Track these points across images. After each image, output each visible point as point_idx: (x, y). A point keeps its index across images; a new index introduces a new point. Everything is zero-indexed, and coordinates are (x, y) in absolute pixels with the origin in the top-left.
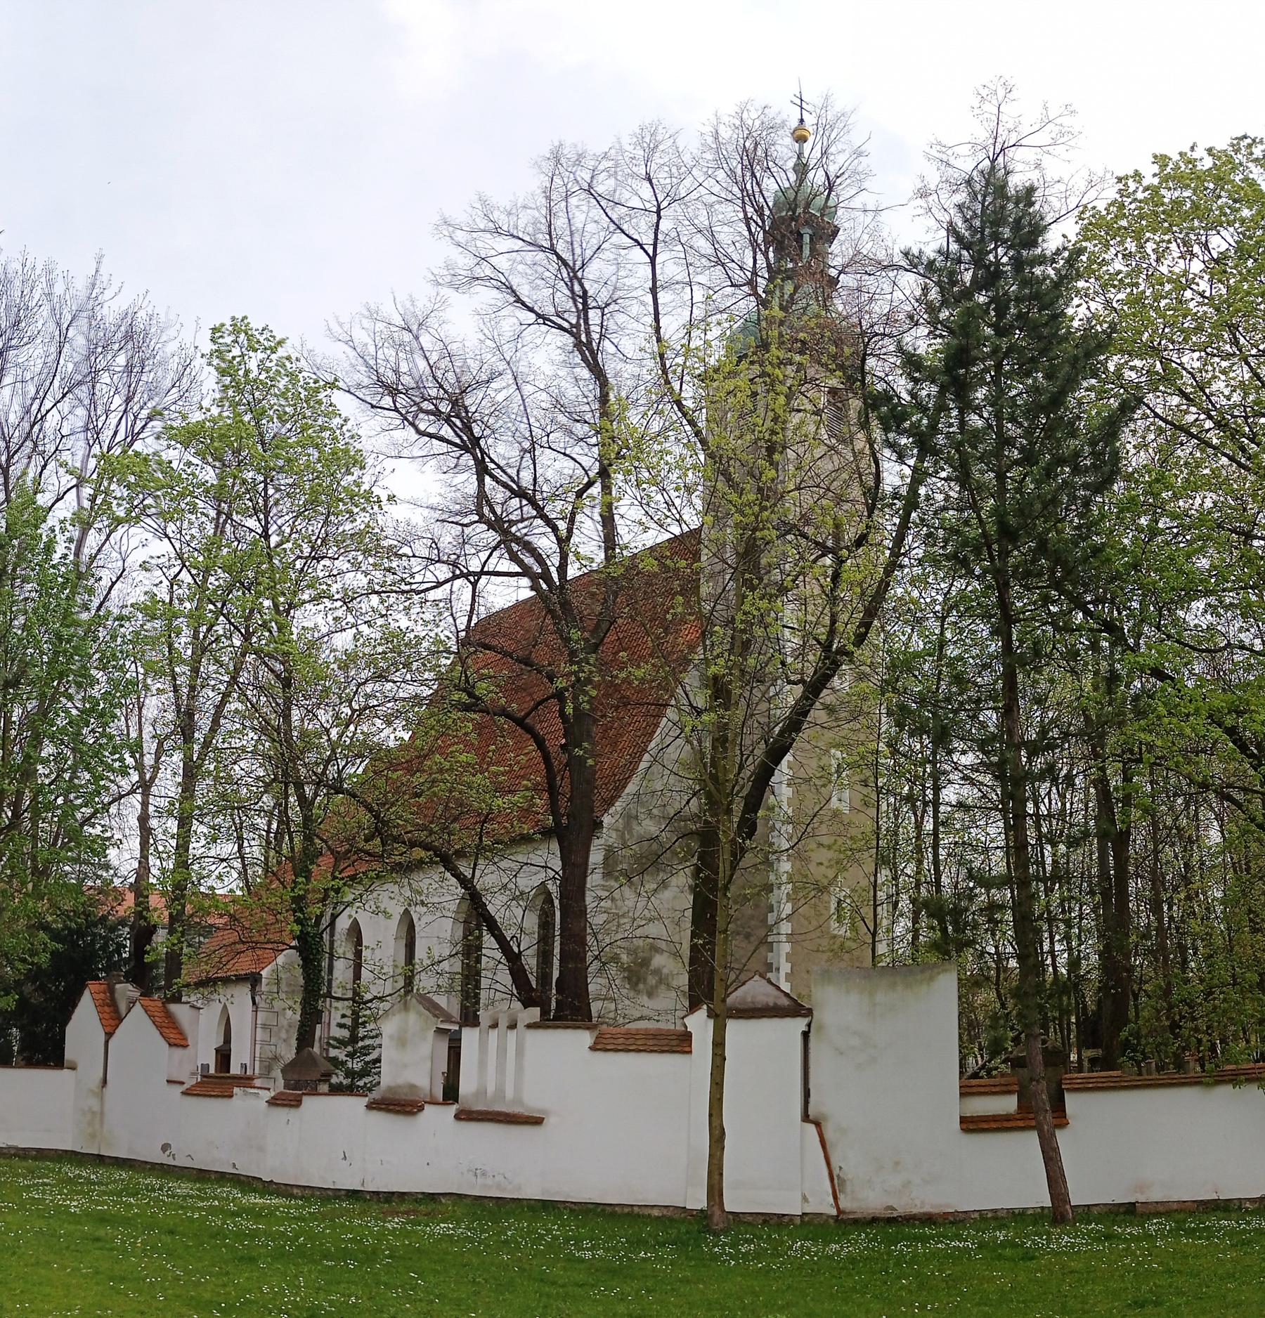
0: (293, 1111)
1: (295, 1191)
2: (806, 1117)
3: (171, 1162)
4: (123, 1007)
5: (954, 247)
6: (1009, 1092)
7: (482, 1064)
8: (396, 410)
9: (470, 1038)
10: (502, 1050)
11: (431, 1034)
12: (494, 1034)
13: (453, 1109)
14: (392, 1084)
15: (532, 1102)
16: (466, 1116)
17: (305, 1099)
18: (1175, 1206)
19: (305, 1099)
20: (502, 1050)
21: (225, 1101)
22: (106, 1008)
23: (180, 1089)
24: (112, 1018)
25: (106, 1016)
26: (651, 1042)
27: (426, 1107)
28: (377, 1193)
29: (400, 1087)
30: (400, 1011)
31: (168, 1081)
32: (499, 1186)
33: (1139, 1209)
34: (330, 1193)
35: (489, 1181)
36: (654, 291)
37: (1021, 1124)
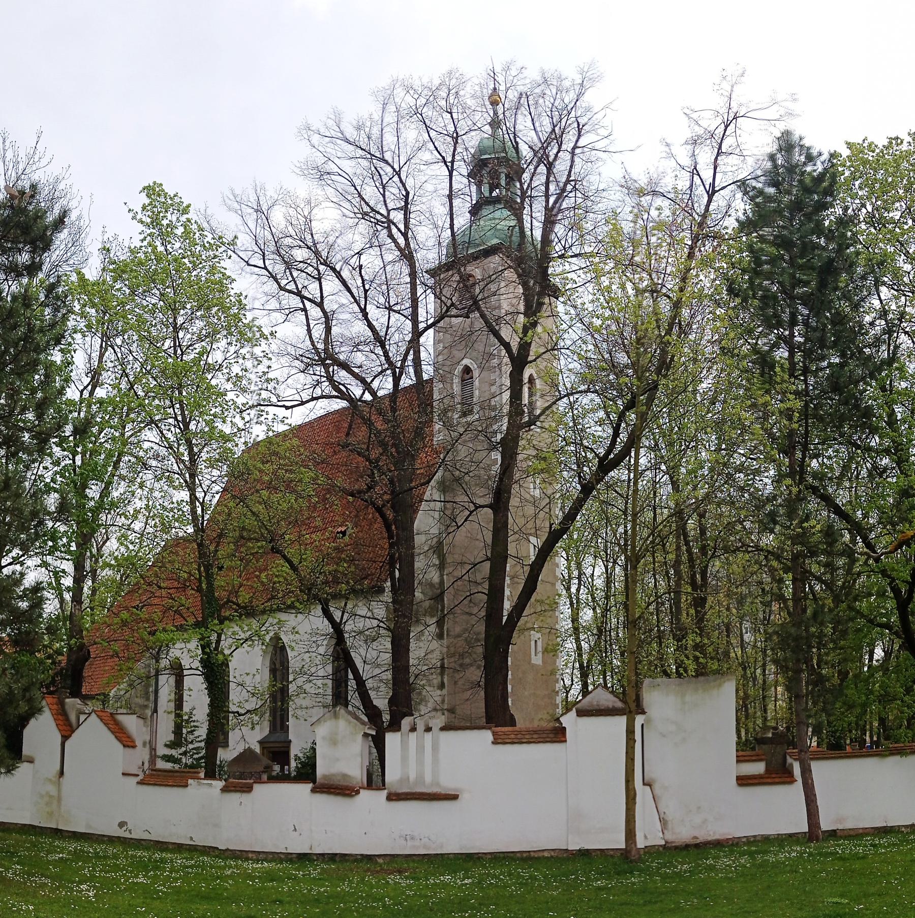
0: (245, 795)
1: (250, 855)
2: (644, 784)
3: (127, 835)
4: (73, 718)
5: (185, 205)
6: (761, 760)
7: (404, 759)
8: (265, 268)
9: (392, 739)
10: (421, 748)
11: (359, 738)
12: (413, 736)
13: (384, 793)
14: (327, 773)
15: (447, 784)
16: (394, 797)
17: (256, 786)
18: (861, 831)
19: (256, 786)
20: (421, 748)
21: (180, 790)
22: (60, 717)
23: (135, 780)
24: (67, 729)
25: (60, 722)
26: (535, 736)
27: (361, 791)
28: (323, 855)
29: (334, 775)
30: (330, 719)
31: (123, 774)
32: (425, 847)
33: (839, 833)
34: (282, 856)
35: (417, 843)
36: (450, 197)
37: (769, 780)
